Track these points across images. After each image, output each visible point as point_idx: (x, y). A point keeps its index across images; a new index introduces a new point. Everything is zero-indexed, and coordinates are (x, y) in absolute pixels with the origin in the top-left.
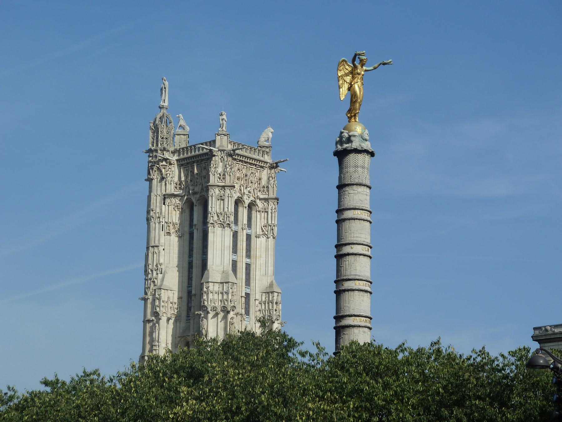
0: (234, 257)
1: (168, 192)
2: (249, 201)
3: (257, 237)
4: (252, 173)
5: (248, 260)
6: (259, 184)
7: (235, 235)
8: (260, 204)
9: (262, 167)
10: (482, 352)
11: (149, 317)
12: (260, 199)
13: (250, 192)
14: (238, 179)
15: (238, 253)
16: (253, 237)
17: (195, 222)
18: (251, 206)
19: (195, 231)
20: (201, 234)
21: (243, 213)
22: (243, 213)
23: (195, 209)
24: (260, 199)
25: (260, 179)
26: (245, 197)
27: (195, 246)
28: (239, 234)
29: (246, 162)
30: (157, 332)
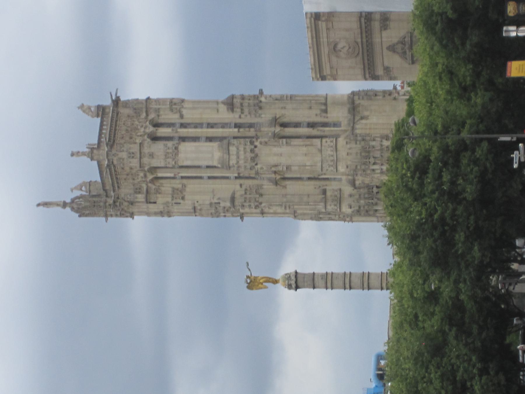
0: (203, 139)
1: (144, 200)
2: (151, 126)
3: (182, 117)
4: (124, 124)
5: (204, 125)
6: (133, 116)
7: (183, 139)
8: (152, 116)
9: (117, 114)
10: (389, 244)
11: (258, 211)
12: (147, 115)
13: (142, 126)
14: (131, 138)
15: (200, 135)
16: (183, 121)
17: (172, 175)
18: (157, 125)
19: (181, 175)
20: (183, 169)
21: (163, 131)
22: (163, 131)
23: (160, 175)
24: (147, 115)
25: (129, 116)
26: (147, 131)
27: (195, 175)
28: (182, 135)
29: (115, 130)
30: (390, 324)
